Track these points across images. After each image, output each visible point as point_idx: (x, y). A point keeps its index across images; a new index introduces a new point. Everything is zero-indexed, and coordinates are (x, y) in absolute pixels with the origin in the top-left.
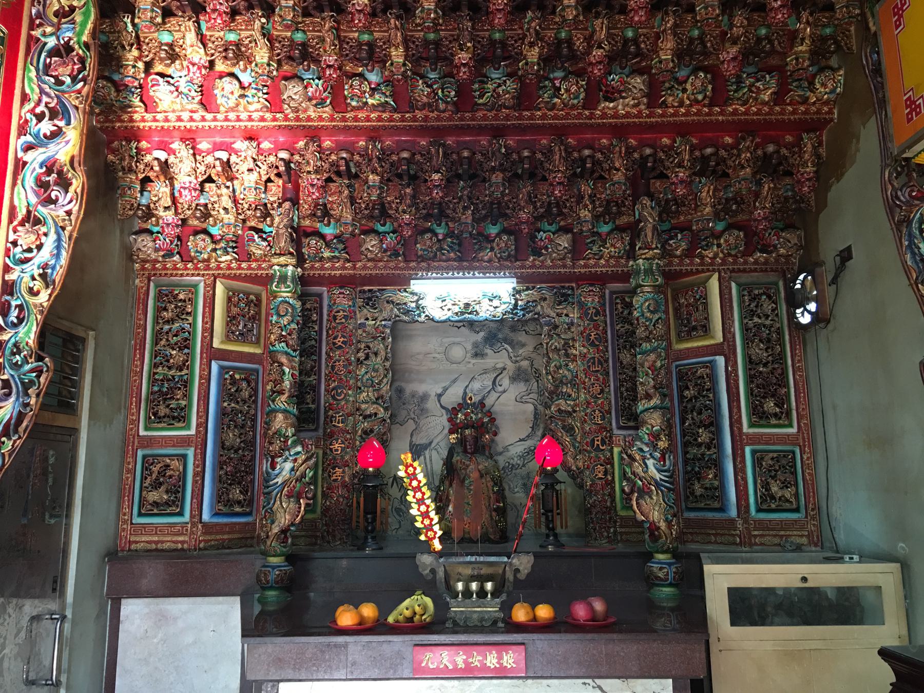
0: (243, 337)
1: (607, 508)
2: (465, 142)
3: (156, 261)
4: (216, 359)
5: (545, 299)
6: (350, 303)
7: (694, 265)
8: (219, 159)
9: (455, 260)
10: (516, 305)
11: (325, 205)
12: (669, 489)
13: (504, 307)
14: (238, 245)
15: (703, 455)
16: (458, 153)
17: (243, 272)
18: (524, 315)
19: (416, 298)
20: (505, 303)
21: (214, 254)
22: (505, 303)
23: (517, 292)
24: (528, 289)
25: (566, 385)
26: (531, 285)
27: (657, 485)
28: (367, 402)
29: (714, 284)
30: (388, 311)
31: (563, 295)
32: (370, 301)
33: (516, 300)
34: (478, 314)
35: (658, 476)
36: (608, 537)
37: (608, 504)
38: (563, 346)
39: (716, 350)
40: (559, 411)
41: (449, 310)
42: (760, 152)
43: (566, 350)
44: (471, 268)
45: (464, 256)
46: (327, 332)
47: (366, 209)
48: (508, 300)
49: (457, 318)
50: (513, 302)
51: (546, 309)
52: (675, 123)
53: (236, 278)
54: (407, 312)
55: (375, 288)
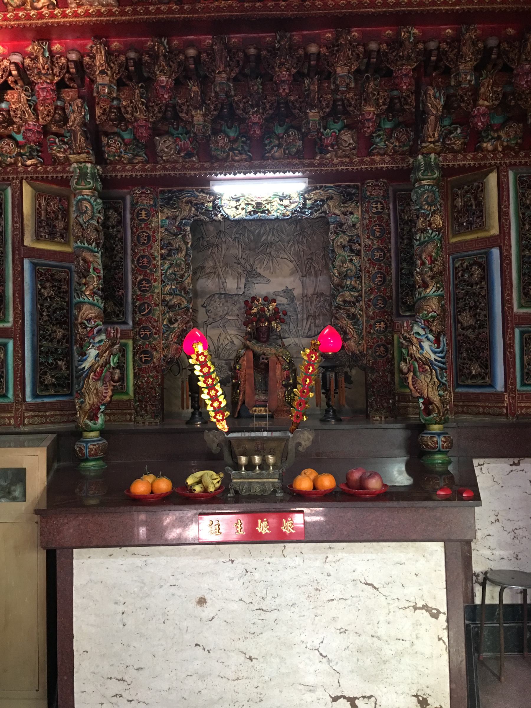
0: (52, 237)
1: (387, 382)
2: (191, 41)
3: (176, 162)
4: (28, 257)
5: (332, 198)
6: (152, 203)
7: (487, 159)
8: (14, 63)
9: (246, 160)
10: (304, 204)
11: (174, 106)
12: (441, 368)
13: (293, 206)
14: (41, 149)
15: (56, 349)
16: (244, 52)
17: (177, 173)
18: (312, 213)
19: (212, 198)
20: (295, 202)
21: (231, 153)
22: (295, 202)
23: (308, 191)
24: (316, 188)
25: (351, 278)
26: (318, 185)
27: (430, 364)
28: (170, 294)
29: (492, 179)
30: (188, 211)
31: (349, 194)
32: (170, 202)
33: (305, 199)
34: (269, 212)
35: (433, 357)
36: (388, 407)
37: (389, 379)
38: (349, 242)
39: (493, 242)
40: (345, 301)
41: (243, 209)
42: (481, 45)
43: (351, 246)
44: (263, 168)
45: (257, 158)
46: (132, 230)
47: (215, 110)
48: (297, 199)
49: (250, 218)
50: (302, 201)
51: (332, 207)
52: (159, 21)
53: (43, 180)
54: (207, 212)
55: (175, 189)
